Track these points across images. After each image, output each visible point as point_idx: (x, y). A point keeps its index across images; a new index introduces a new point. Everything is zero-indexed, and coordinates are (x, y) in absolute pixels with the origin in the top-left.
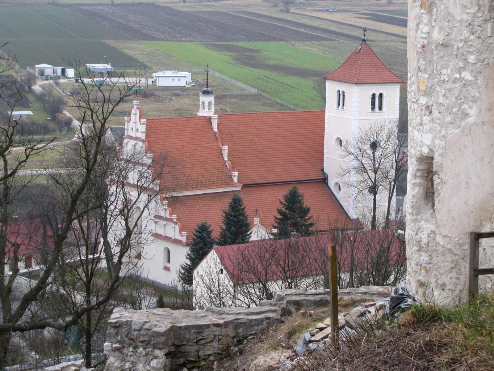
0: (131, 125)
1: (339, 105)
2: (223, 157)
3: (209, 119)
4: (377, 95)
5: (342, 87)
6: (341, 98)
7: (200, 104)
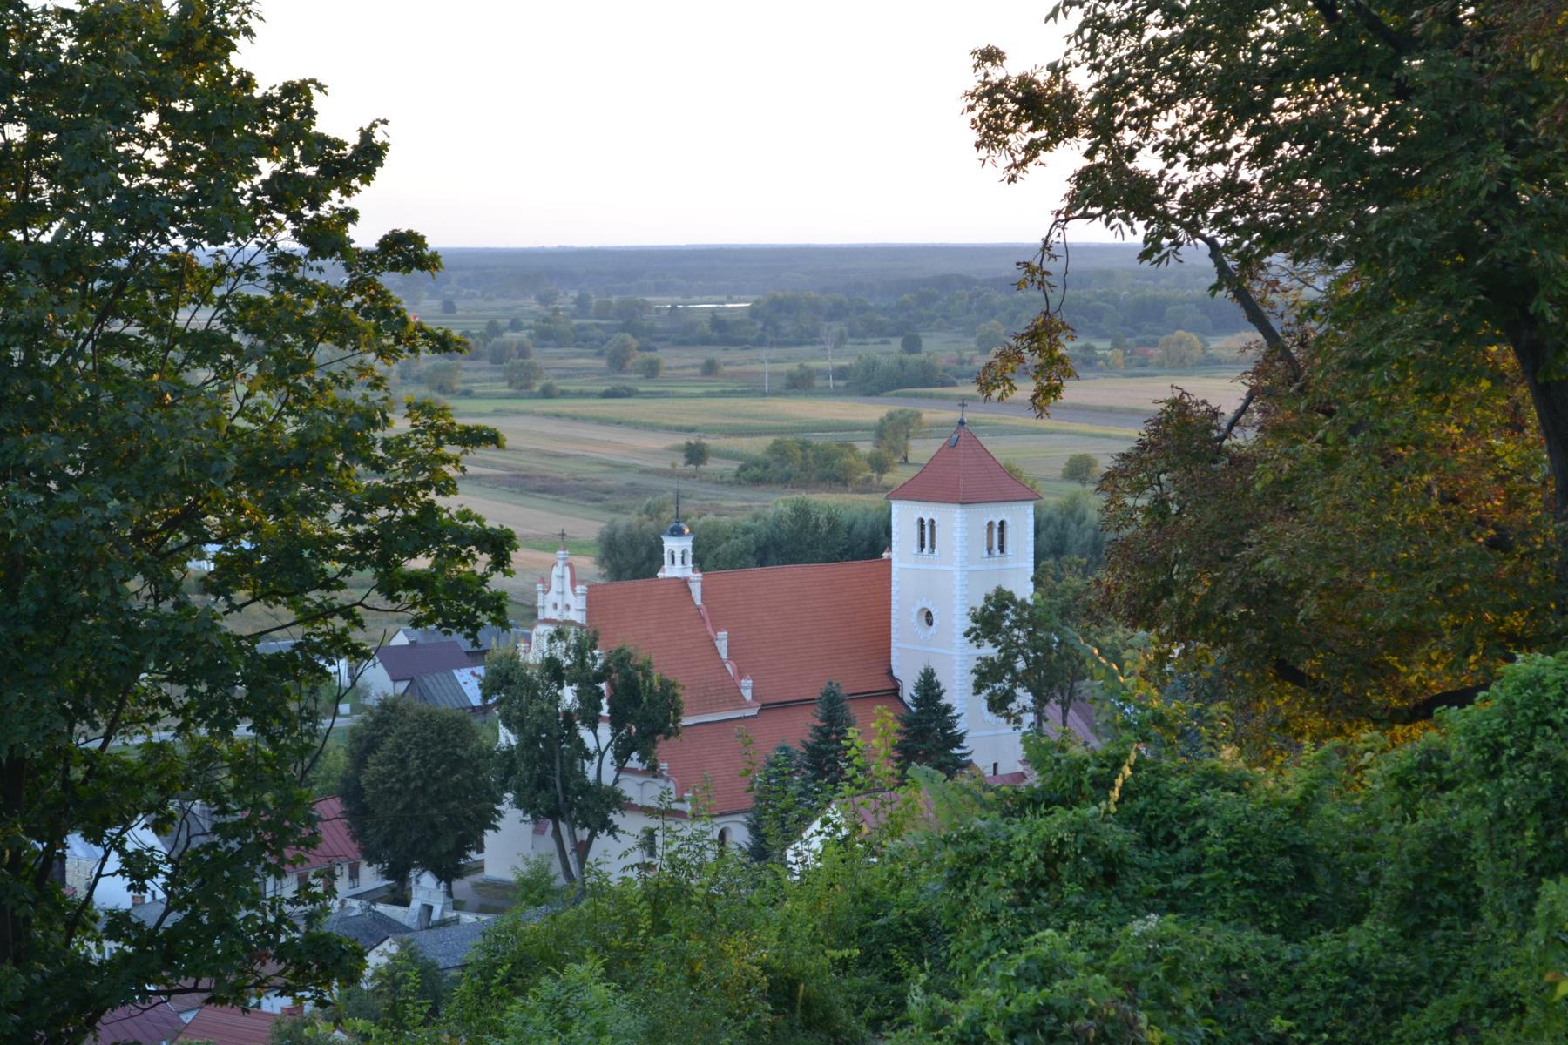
0: (552, 596)
1: (922, 546)
2: (718, 654)
3: (685, 582)
4: (926, 550)
5: (928, 511)
6: (926, 534)
7: (666, 554)
